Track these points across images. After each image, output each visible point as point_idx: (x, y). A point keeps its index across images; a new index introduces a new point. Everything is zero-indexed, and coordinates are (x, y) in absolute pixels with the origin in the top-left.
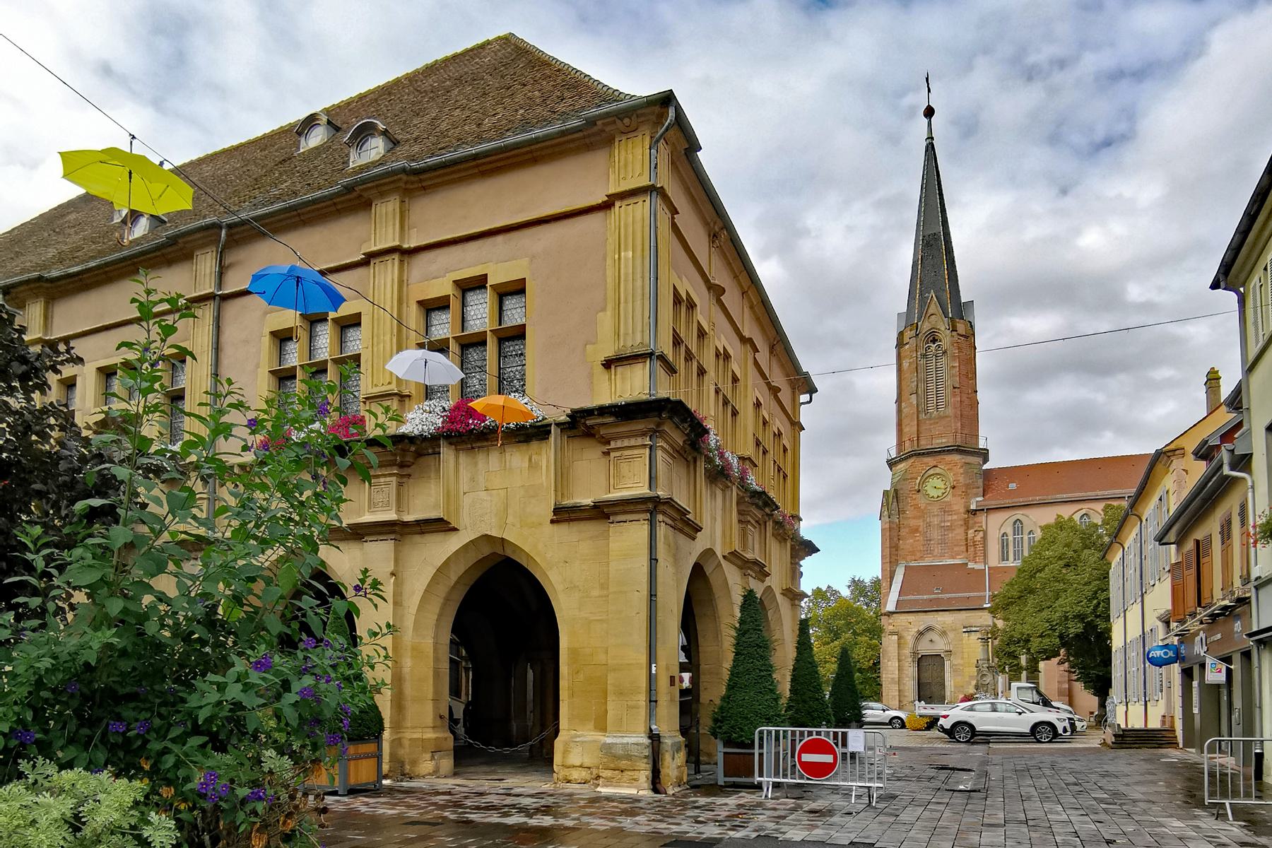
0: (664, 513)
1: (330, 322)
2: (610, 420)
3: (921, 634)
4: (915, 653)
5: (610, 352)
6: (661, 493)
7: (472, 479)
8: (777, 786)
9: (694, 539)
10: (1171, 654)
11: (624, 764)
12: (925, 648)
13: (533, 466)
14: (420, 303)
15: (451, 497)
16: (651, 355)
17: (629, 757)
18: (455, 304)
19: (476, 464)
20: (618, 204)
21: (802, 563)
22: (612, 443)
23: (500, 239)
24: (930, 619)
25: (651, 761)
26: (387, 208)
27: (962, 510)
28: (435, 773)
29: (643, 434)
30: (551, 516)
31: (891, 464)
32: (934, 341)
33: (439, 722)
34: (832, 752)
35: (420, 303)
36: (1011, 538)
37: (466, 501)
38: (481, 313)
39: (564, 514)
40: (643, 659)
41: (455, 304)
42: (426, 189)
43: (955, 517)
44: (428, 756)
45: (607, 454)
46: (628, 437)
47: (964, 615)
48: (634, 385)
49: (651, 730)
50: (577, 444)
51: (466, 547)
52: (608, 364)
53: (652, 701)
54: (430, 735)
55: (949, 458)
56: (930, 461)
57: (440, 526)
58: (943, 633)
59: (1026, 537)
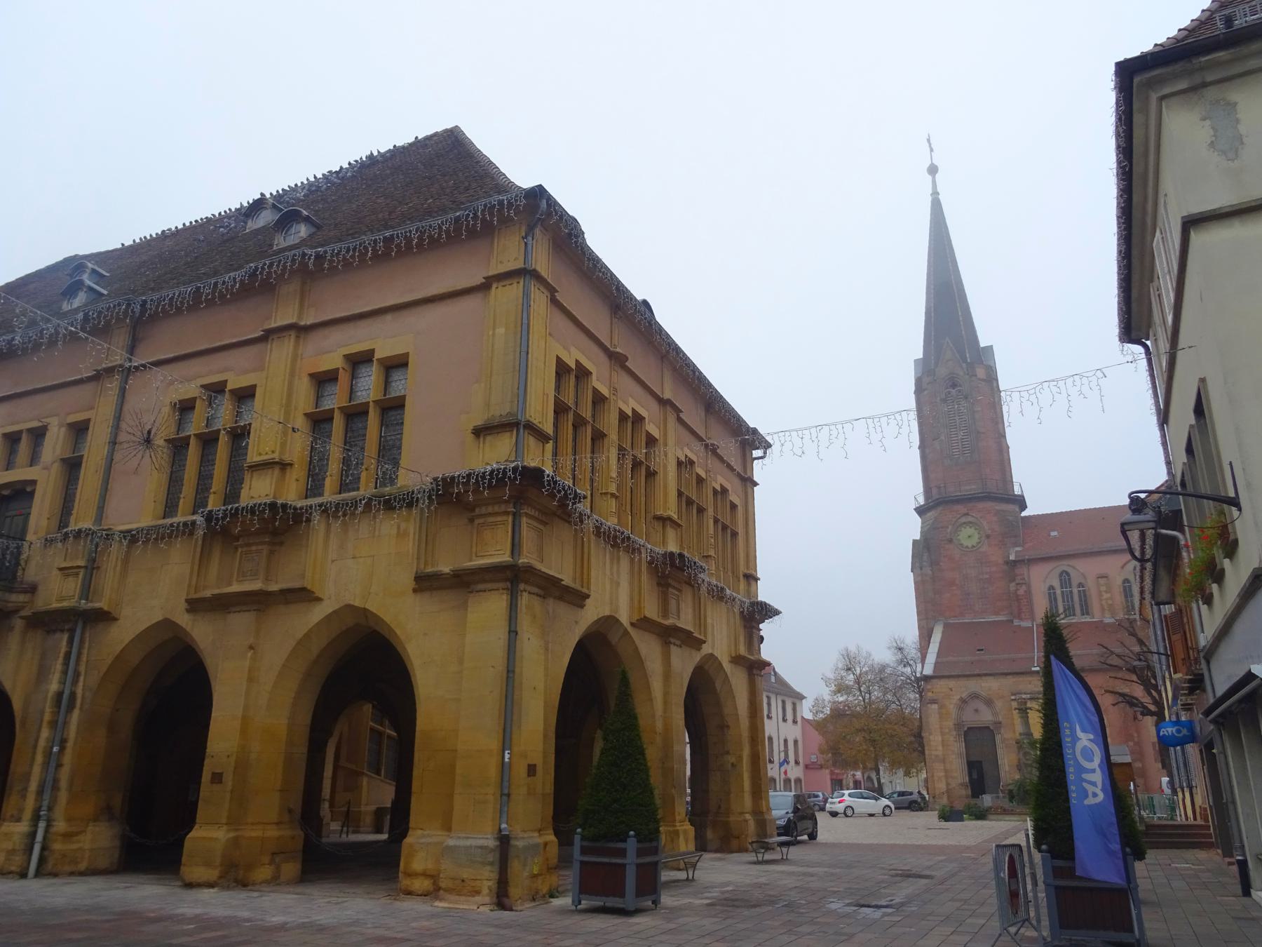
1: (227, 395)
3: (964, 701)
4: (958, 726)
5: (479, 422)
6: (522, 561)
9: (582, 606)
10: (1185, 731)
12: (971, 719)
13: (401, 535)
14: (312, 376)
18: (344, 378)
20: (494, 286)
21: (761, 626)
22: (477, 510)
23: (389, 317)
24: (974, 685)
25: (496, 868)
26: (290, 289)
27: (1001, 561)
31: (920, 511)
32: (954, 386)
35: (312, 376)
36: (1058, 592)
38: (369, 386)
39: (426, 583)
40: (494, 744)
41: (344, 378)
43: (994, 569)
44: (266, 859)
45: (471, 520)
47: (1010, 681)
48: (497, 455)
49: (500, 830)
51: (329, 618)
52: (479, 432)
53: (505, 796)
54: (273, 832)
55: (981, 505)
56: (961, 508)
58: (989, 702)
59: (1075, 591)
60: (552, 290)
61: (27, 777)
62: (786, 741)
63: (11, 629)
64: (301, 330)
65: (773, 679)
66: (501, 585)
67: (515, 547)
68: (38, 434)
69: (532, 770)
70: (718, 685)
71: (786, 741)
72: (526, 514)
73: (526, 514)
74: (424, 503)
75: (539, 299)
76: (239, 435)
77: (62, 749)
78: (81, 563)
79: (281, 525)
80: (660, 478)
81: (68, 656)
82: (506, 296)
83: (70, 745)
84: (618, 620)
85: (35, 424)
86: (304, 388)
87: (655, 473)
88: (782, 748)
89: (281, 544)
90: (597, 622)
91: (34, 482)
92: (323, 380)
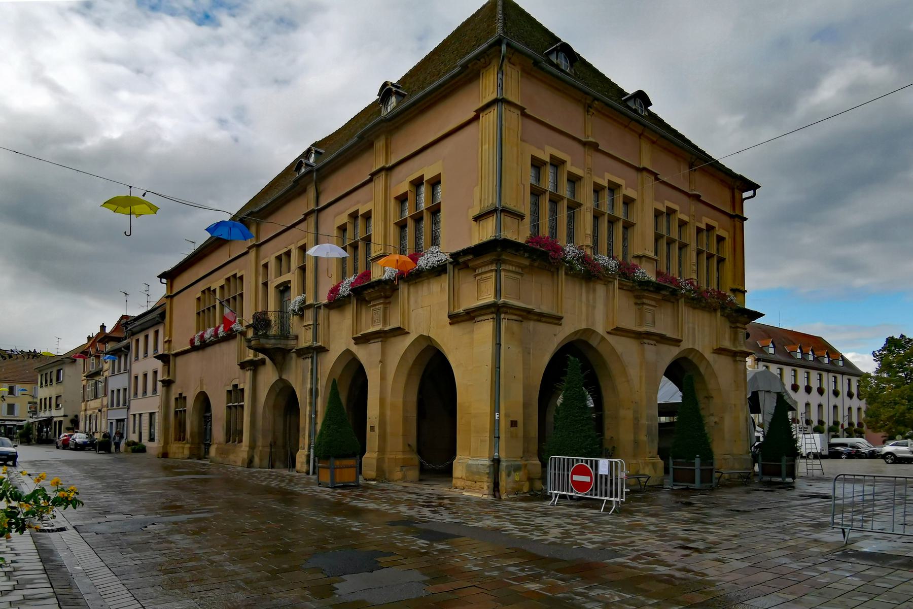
0: (506, 313)
2: (470, 257)
5: (476, 211)
7: (416, 302)
8: (562, 497)
11: (477, 477)
13: (442, 289)
15: (405, 315)
16: (495, 211)
17: (479, 473)
18: (411, 197)
19: (594, 290)
28: (404, 479)
29: (491, 263)
30: (563, 321)
33: (408, 448)
34: (590, 474)
35: (396, 198)
37: (413, 315)
39: (455, 319)
42: (398, 128)
44: (398, 469)
46: (485, 266)
48: (487, 232)
50: (462, 274)
52: (477, 219)
57: (399, 332)
60: (522, 110)
61: (304, 428)
62: (850, 409)
63: (291, 358)
64: (389, 170)
65: (841, 363)
66: (491, 316)
67: (498, 292)
68: (288, 254)
69: (514, 424)
70: (702, 370)
71: (850, 409)
72: (504, 270)
73: (504, 270)
74: (450, 268)
75: (512, 117)
76: (368, 240)
77: (316, 415)
78: (311, 323)
79: (387, 290)
80: (637, 229)
81: (312, 369)
82: (490, 118)
83: (319, 413)
84: (594, 331)
85: (286, 250)
86: (392, 205)
87: (633, 225)
88: (846, 413)
89: (390, 303)
90: (576, 333)
91: (290, 282)
92: (402, 199)
